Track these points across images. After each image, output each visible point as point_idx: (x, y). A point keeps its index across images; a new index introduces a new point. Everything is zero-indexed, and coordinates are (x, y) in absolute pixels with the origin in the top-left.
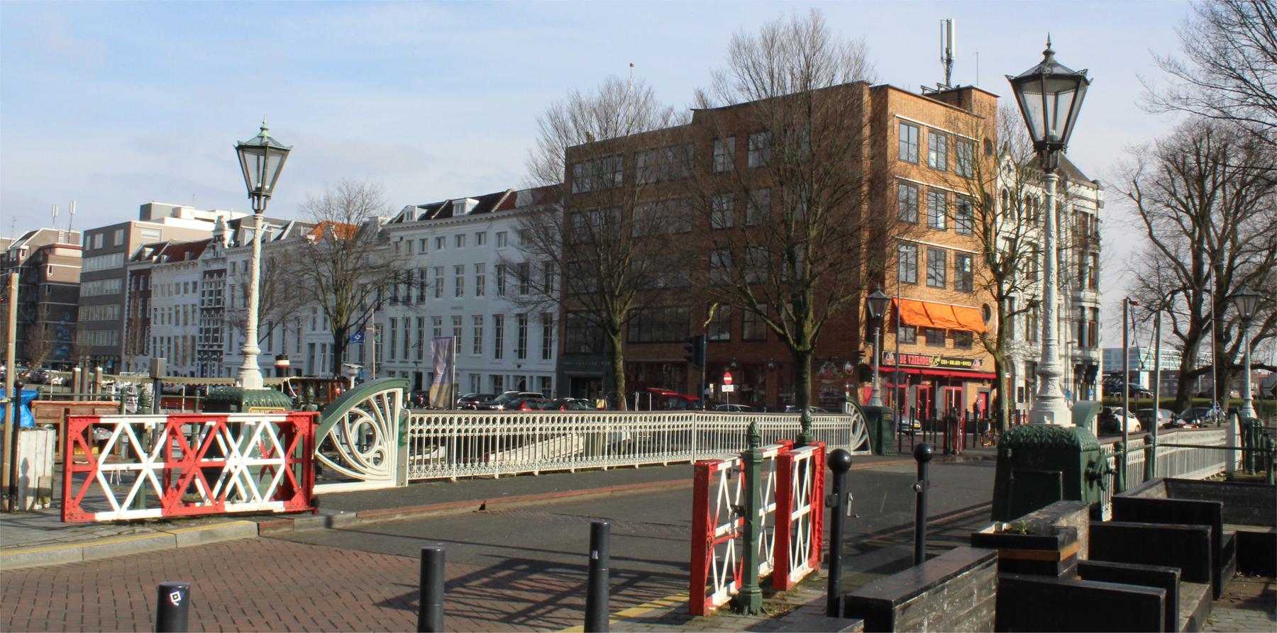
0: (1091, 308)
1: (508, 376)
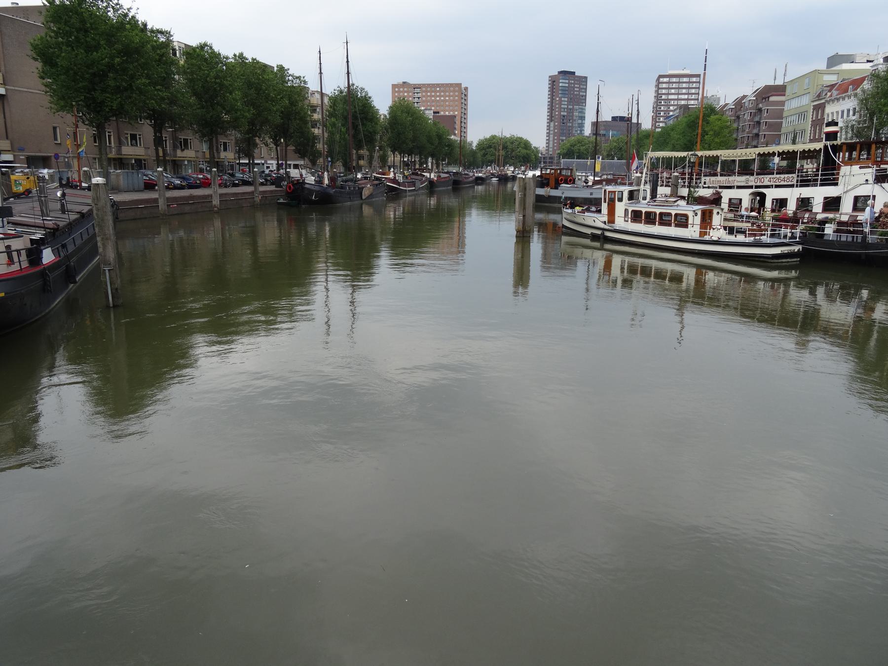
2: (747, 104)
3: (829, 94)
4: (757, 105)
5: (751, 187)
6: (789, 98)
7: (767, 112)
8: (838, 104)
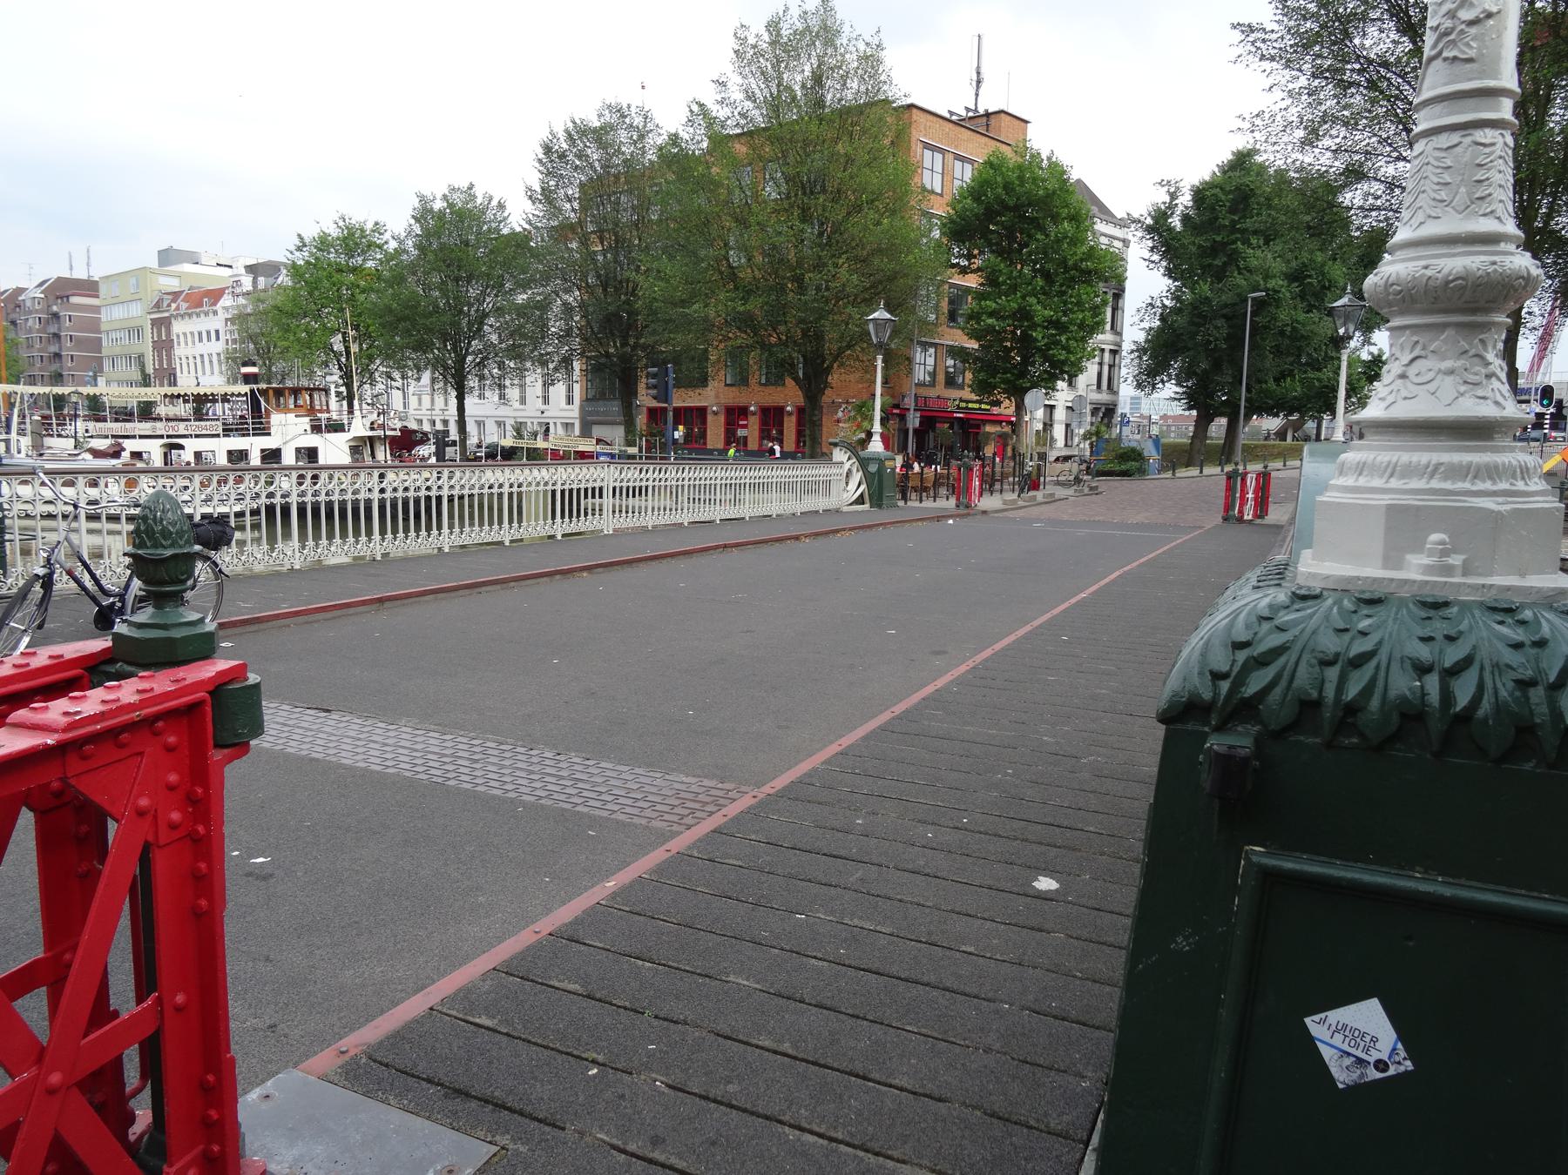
0: (1111, 350)
1: (555, 423)
2: (28, 304)
3: (174, 306)
4: (49, 306)
5: (161, 437)
6: (105, 303)
7: (70, 320)
8: (191, 321)
